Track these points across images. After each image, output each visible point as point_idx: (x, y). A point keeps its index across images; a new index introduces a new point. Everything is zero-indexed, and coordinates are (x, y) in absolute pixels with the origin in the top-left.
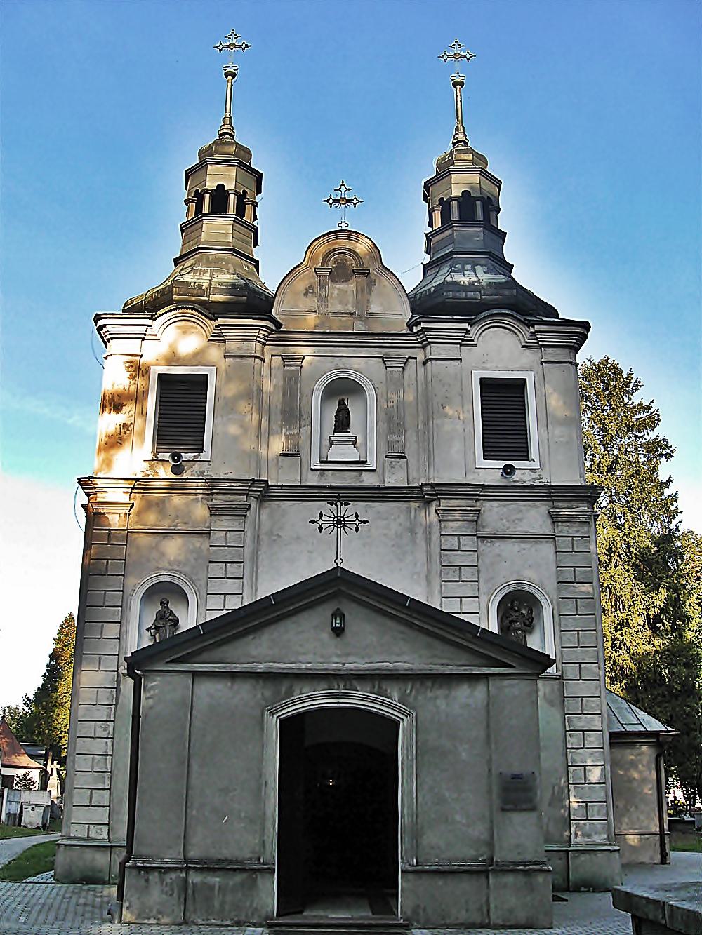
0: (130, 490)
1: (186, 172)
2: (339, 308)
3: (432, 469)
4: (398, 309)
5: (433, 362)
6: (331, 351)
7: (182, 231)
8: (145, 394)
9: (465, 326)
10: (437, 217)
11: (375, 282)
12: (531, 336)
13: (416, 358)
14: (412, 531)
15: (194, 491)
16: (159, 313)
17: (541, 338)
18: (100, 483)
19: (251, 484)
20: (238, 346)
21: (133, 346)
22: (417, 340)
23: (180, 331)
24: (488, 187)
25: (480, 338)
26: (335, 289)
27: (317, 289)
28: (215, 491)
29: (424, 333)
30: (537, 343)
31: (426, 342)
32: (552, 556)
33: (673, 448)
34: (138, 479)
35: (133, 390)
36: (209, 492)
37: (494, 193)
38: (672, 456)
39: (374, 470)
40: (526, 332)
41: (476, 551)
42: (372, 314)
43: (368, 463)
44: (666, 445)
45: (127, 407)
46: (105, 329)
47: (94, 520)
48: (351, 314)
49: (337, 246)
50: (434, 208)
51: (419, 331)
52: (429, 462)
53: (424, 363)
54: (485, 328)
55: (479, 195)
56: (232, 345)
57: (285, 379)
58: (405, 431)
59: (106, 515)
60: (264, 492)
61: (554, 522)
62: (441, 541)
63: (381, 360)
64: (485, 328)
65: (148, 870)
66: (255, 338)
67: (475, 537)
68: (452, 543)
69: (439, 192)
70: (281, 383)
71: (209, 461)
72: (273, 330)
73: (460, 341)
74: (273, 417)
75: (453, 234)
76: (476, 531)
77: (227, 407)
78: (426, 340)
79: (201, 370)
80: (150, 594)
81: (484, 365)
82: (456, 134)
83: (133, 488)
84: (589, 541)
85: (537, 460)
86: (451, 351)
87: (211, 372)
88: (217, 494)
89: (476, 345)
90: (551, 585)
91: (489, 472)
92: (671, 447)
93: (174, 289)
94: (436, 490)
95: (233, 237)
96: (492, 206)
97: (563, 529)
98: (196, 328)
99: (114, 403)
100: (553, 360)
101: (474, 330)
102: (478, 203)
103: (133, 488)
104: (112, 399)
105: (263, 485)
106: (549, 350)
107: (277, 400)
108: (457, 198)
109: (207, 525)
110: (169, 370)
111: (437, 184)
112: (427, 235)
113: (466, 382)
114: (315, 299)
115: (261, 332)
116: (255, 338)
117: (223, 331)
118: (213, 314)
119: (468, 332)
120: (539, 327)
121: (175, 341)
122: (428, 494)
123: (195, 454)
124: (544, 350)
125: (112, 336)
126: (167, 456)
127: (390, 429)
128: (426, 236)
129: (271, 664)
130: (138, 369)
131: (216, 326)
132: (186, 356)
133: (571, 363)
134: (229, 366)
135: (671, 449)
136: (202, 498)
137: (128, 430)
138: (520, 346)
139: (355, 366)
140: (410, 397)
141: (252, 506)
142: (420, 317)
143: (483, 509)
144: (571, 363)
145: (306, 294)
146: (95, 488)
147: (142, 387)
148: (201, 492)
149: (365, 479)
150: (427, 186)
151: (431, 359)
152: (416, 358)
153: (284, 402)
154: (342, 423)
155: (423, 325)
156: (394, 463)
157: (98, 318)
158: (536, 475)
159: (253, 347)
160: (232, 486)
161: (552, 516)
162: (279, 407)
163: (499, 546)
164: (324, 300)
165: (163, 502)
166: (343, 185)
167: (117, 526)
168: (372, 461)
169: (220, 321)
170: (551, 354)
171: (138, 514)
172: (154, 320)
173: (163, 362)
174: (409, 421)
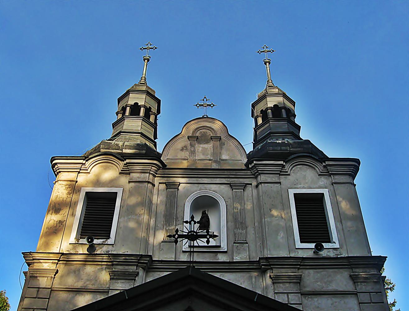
0: (57, 261)
1: (118, 99)
2: (202, 157)
3: (266, 250)
4: (239, 157)
6: (197, 180)
7: (113, 128)
8: (76, 203)
11: (224, 143)
12: (324, 168)
13: (251, 184)
15: (100, 263)
17: (330, 169)
18: (37, 256)
19: (140, 258)
20: (138, 176)
21: (72, 176)
22: (252, 173)
23: (102, 168)
24: (288, 104)
25: (292, 171)
26: (200, 147)
27: (189, 147)
28: (114, 263)
29: (256, 168)
30: (328, 172)
31: (258, 173)
33: (394, 284)
34: (63, 254)
35: (69, 200)
36: (111, 264)
37: (292, 108)
38: (393, 289)
39: (226, 252)
41: (301, 304)
43: (222, 247)
44: (390, 283)
45: (63, 210)
46: (56, 166)
47: (29, 281)
48: (210, 160)
49: (201, 125)
50: (257, 115)
51: (253, 167)
52: (263, 245)
53: (257, 186)
54: (294, 165)
55: (283, 106)
56: (135, 176)
57: (167, 197)
58: (246, 228)
59: (38, 278)
61: (355, 283)
63: (229, 185)
64: (294, 165)
66: (149, 171)
69: (260, 107)
71: (113, 245)
72: (161, 168)
73: (279, 172)
74: (159, 219)
75: (270, 125)
76: (300, 290)
77: (129, 211)
79: (113, 190)
81: (296, 186)
82: (267, 84)
83: (59, 260)
84: (382, 295)
85: (337, 242)
86: (275, 178)
87: (119, 191)
92: (392, 283)
93: (101, 146)
95: (141, 128)
96: (291, 114)
97: (362, 287)
98: (113, 167)
99: (57, 208)
101: (288, 167)
102: (283, 110)
103: (59, 260)
104: (55, 206)
105: (148, 259)
106: (336, 177)
107: (162, 209)
108: (271, 108)
109: (107, 286)
111: (260, 104)
113: (284, 196)
114: (188, 153)
115: (152, 168)
116: (149, 171)
117: (128, 167)
119: (283, 166)
120: (328, 162)
121: (99, 174)
122: (263, 265)
123: (104, 240)
124: (333, 177)
126: (84, 241)
127: (236, 225)
130: (74, 187)
131: (125, 164)
132: (105, 182)
133: (351, 183)
134: (131, 187)
135: (393, 285)
136: (106, 268)
137: (62, 224)
139: (213, 189)
140: (249, 206)
143: (303, 275)
144: (351, 183)
146: (34, 259)
147: (75, 200)
148: (105, 263)
149: (220, 258)
150: (253, 106)
151: (261, 183)
152: (251, 184)
153: (166, 210)
156: (239, 247)
157: (53, 159)
158: (338, 252)
159: (146, 177)
160: (127, 259)
161: (354, 279)
162: (163, 213)
164: (193, 153)
165: (79, 270)
166: (206, 98)
167: (45, 285)
168: (224, 247)
170: (338, 179)
171: (62, 277)
172: (87, 161)
173: (90, 185)
174: (249, 221)
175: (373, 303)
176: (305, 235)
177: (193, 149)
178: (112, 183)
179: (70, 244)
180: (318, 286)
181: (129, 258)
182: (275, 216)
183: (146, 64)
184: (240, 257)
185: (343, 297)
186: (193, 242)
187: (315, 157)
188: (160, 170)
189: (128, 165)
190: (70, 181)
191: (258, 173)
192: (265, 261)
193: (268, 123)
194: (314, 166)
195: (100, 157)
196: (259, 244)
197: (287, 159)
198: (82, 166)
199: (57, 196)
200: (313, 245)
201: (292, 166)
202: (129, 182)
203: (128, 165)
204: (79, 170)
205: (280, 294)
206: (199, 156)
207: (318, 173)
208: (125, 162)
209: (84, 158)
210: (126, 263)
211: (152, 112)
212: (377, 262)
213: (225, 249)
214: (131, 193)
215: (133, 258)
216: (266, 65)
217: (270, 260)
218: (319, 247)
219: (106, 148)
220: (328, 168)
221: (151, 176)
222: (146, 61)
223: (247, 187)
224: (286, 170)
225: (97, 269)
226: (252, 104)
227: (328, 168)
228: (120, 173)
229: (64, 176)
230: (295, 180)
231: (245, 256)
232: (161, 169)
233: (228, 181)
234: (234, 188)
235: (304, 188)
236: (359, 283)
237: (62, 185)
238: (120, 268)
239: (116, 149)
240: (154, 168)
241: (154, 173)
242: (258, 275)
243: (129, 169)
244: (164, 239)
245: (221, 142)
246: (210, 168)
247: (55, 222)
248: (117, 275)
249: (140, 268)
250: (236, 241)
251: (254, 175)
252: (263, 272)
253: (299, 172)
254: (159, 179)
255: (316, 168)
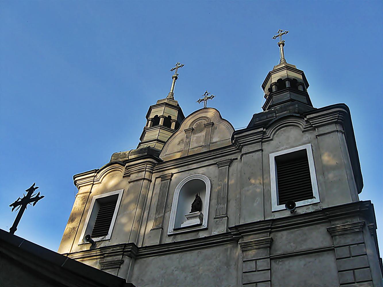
6: (188, 168)
12: (306, 123)
14: (228, 264)
15: (95, 257)
17: (313, 122)
20: (136, 176)
21: (87, 189)
28: (105, 255)
30: (312, 126)
36: (103, 256)
40: (303, 124)
54: (277, 129)
56: (133, 177)
61: (332, 237)
62: (243, 266)
67: (269, 259)
68: (252, 266)
70: (159, 192)
72: (155, 164)
78: (240, 145)
81: (278, 149)
86: (257, 147)
88: (107, 256)
94: (239, 230)
97: (341, 241)
101: (269, 132)
105: (131, 247)
106: (321, 129)
108: (275, 84)
110: (101, 196)
112: (263, 108)
121: (109, 182)
122: (234, 235)
124: (318, 129)
125: (79, 184)
128: (263, 108)
131: (126, 168)
137: (75, 230)
138: (301, 132)
139: (201, 172)
141: (125, 262)
148: (99, 257)
161: (331, 232)
172: (98, 173)
175: (353, 257)
178: (116, 187)
179: (78, 245)
180: (290, 248)
181: (115, 249)
182: (253, 184)
183: (173, 81)
184: (218, 231)
185: (318, 255)
187: (296, 115)
188: (156, 166)
189: (127, 168)
190: (86, 193)
191: (241, 146)
192: (235, 230)
193: (272, 98)
195: (106, 168)
196: (238, 215)
197: (268, 124)
198: (94, 178)
199: (75, 207)
201: (275, 130)
202: (129, 182)
203: (127, 168)
204: (92, 182)
205: (248, 262)
207: (302, 130)
209: (95, 171)
210: (115, 254)
211: (172, 119)
212: (358, 209)
213: (205, 226)
214: (129, 192)
215: (118, 248)
216: (280, 47)
217: (239, 228)
218: (291, 205)
219: (116, 158)
220: (310, 122)
221: (147, 173)
222: (174, 79)
223: (234, 162)
224: (267, 136)
225: (93, 263)
226: (262, 86)
227: (310, 122)
228: (124, 177)
229: (83, 190)
230: (277, 144)
231: (222, 229)
232: (156, 165)
233: (215, 161)
235: (286, 148)
236: (337, 237)
237: (80, 198)
238: (109, 259)
239: (124, 157)
240: (149, 165)
241: (150, 170)
242: (232, 247)
243: (129, 171)
244: (153, 227)
245: (213, 127)
247: (71, 229)
248: (264, 243)
249: (127, 257)
250: (217, 217)
251: (239, 149)
252: (236, 241)
253: (282, 135)
254: (156, 175)
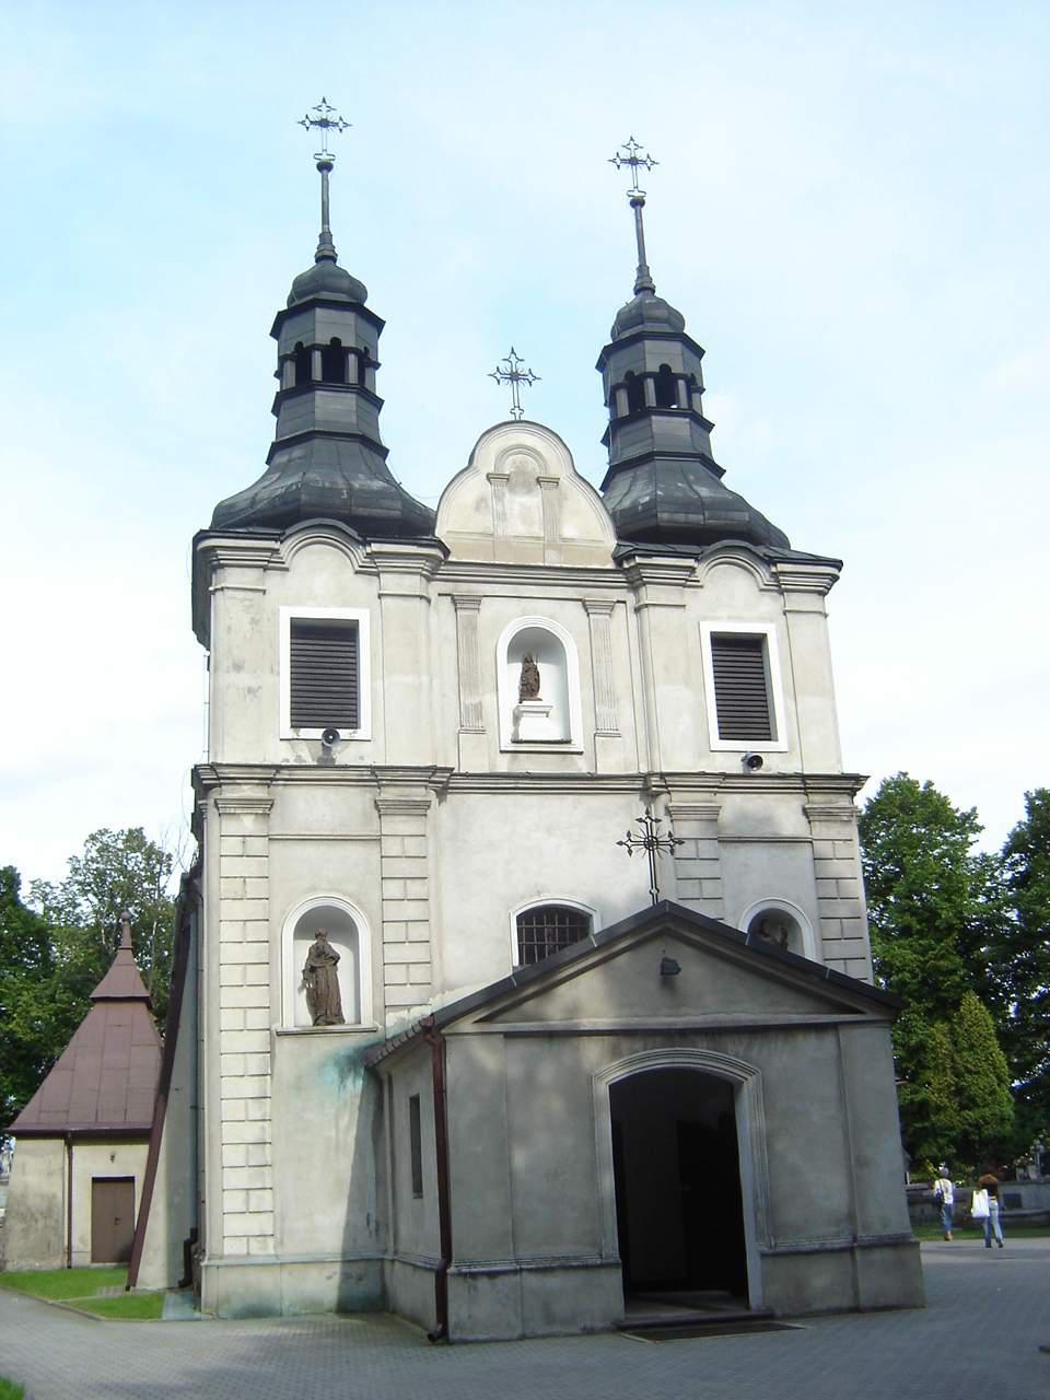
5: (651, 609)
9: (690, 562)
10: (622, 397)
16: (288, 532)
32: (808, 865)
40: (764, 574)
42: (564, 540)
52: (216, 756)
60: (444, 782)
65: (473, 1275)
80: (306, 927)
89: (701, 587)
90: (811, 902)
91: (728, 756)
100: (797, 609)
101: (701, 569)
102: (681, 383)
118: (364, 537)
119: (692, 570)
129: (716, 1015)
142: (636, 549)
145: (477, 509)
152: (624, 602)
154: (530, 688)
155: (638, 560)
163: (744, 852)
169: (375, 547)
172: (282, 542)
176: (754, 665)
177: (499, 508)
186: (320, 737)
194: (752, 569)
200: (318, 733)
206: (516, 527)
208: (369, 550)
234: (594, 611)
246: (542, 564)
255: (758, 576)
